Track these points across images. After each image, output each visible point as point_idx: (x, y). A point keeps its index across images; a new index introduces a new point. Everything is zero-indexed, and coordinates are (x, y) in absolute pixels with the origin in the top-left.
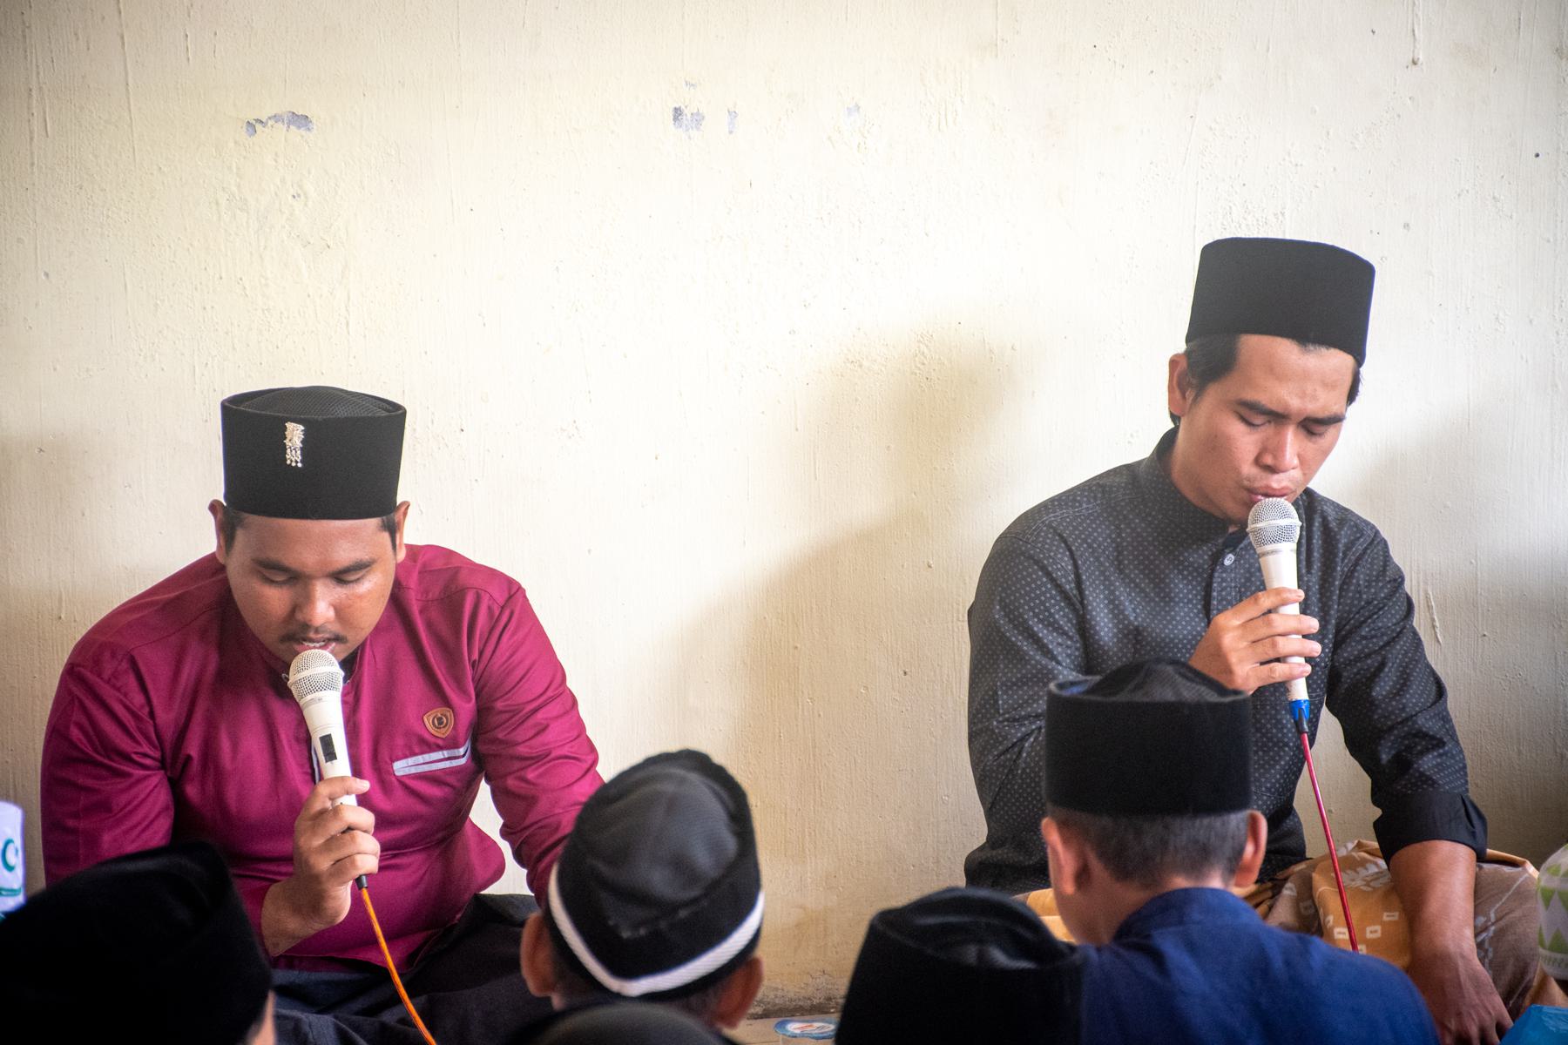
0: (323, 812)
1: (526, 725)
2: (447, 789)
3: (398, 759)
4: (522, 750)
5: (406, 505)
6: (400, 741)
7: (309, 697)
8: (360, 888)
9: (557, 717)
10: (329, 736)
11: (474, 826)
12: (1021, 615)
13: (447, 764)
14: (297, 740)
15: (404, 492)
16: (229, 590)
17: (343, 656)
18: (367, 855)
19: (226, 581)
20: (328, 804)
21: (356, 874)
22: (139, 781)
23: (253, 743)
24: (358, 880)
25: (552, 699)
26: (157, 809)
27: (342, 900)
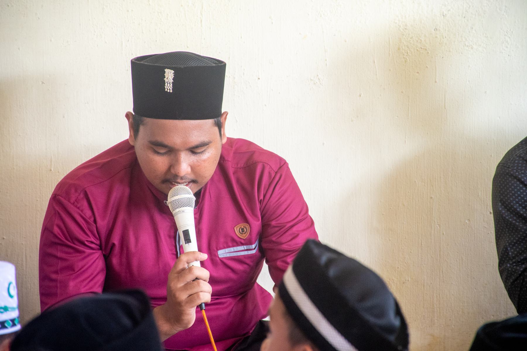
0: (183, 270)
1: (287, 234)
2: (246, 266)
3: (221, 249)
4: (285, 247)
5: (226, 113)
6: (222, 240)
7: (177, 210)
8: (201, 309)
9: (304, 230)
10: (188, 230)
11: (258, 285)
12: (512, 206)
13: (246, 253)
14: (170, 237)
15: (227, 105)
16: (136, 159)
17: (196, 190)
18: (206, 293)
19: (134, 153)
20: (186, 266)
21: (199, 302)
22: (88, 255)
23: (146, 238)
24: (199, 307)
25: (301, 221)
26: (98, 269)
27: (191, 316)
